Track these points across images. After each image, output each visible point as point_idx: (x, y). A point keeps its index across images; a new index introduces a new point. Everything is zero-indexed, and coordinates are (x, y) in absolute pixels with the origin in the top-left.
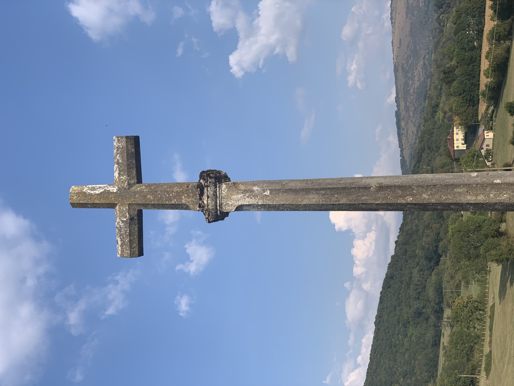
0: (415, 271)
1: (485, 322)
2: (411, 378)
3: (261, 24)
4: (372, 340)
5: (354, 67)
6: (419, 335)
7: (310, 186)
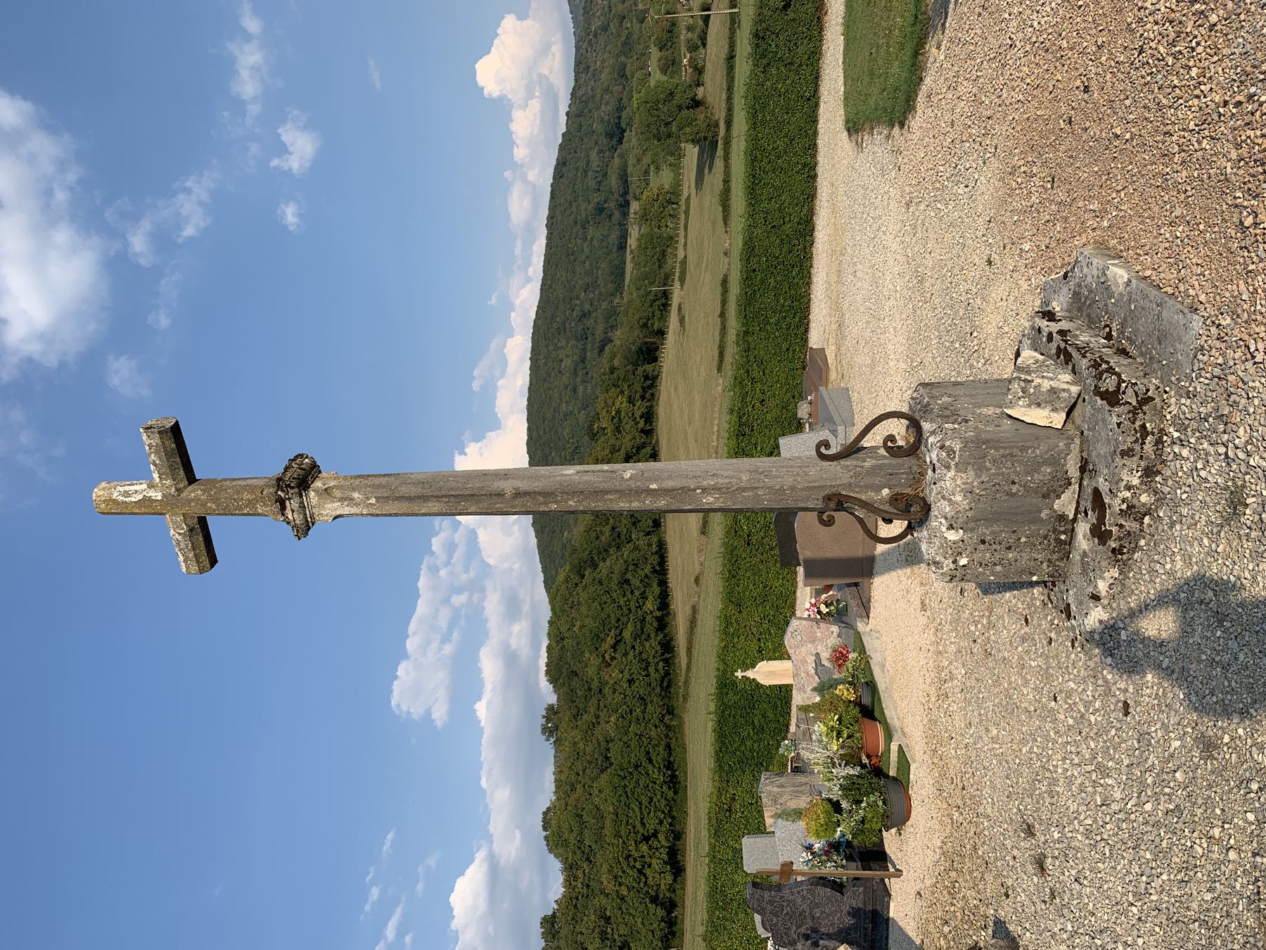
0: (594, 154)
6: (601, 237)
7: (428, 492)
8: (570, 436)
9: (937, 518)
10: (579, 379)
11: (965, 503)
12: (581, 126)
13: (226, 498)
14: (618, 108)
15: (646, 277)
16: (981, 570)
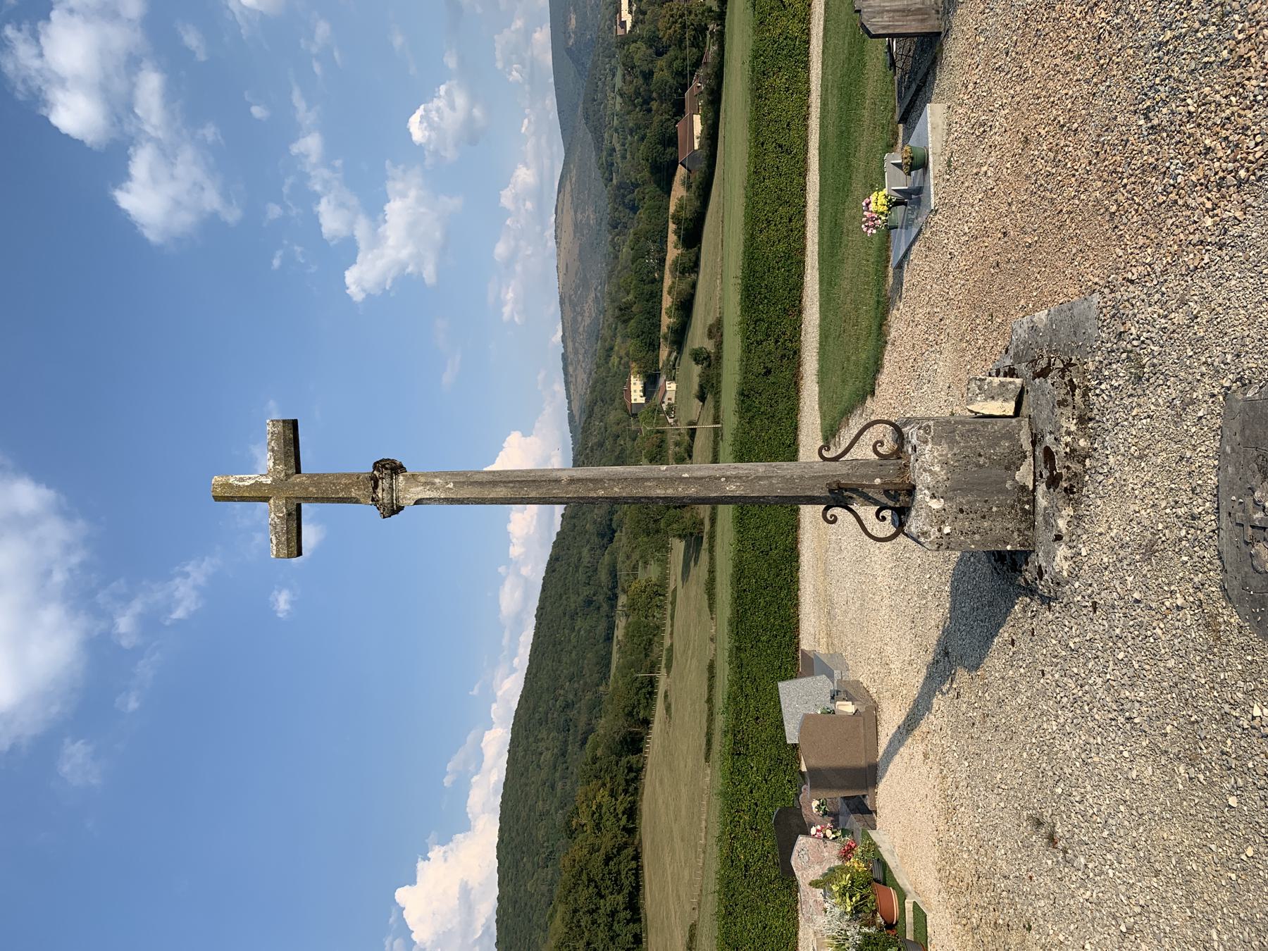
0: (585, 551)
1: (665, 610)
2: (579, 682)
3: (388, 233)
4: (532, 637)
5: (510, 295)
8: (545, 839)
9: (922, 490)
10: (558, 775)
11: (942, 473)
12: (575, 526)
13: (326, 483)
15: (632, 665)
16: (962, 538)
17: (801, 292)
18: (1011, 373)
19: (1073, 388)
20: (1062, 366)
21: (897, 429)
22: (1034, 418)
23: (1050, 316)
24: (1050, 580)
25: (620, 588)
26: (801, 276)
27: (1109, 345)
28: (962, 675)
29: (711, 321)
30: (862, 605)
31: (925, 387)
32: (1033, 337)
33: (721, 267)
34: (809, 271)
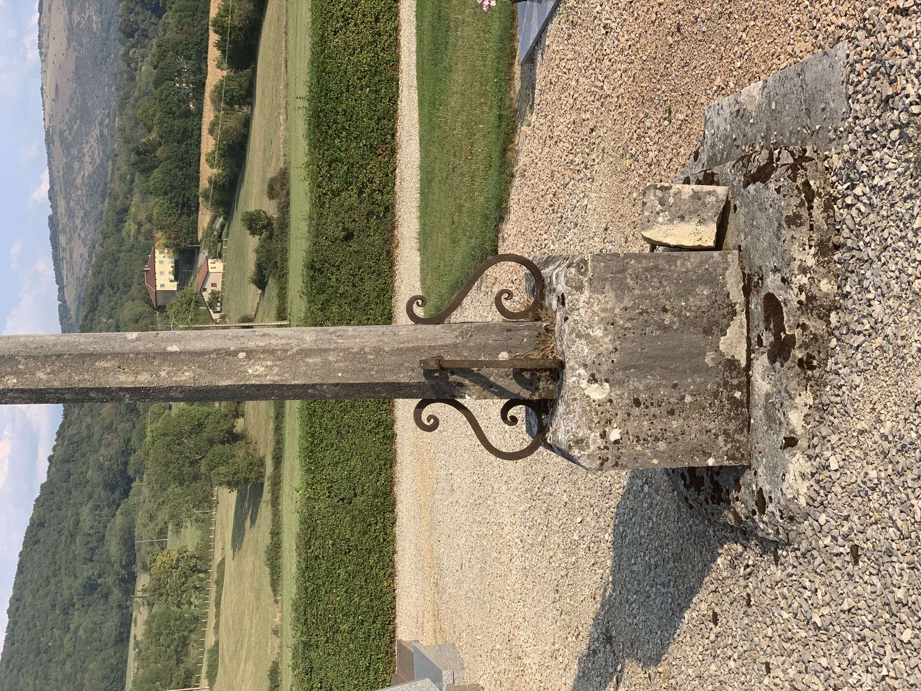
0: (85, 511)
6: (90, 626)
11: (607, 340)
14: (123, 451)
16: (639, 448)
17: (395, 123)
18: (709, 179)
19: (810, 195)
20: (791, 161)
21: (534, 271)
22: (747, 250)
23: (766, 90)
24: (778, 513)
25: (139, 564)
26: (394, 99)
27: (868, 121)
28: (633, 672)
29: (272, 173)
30: (482, 569)
31: (570, 235)
32: (739, 127)
33: (286, 97)
34: (404, 92)
